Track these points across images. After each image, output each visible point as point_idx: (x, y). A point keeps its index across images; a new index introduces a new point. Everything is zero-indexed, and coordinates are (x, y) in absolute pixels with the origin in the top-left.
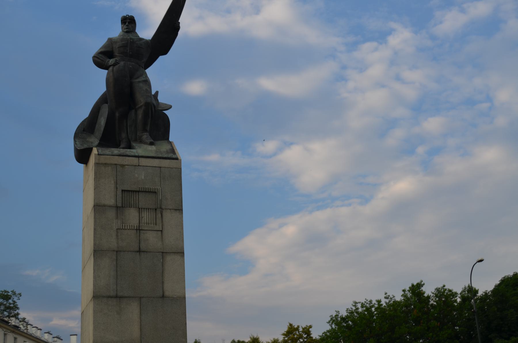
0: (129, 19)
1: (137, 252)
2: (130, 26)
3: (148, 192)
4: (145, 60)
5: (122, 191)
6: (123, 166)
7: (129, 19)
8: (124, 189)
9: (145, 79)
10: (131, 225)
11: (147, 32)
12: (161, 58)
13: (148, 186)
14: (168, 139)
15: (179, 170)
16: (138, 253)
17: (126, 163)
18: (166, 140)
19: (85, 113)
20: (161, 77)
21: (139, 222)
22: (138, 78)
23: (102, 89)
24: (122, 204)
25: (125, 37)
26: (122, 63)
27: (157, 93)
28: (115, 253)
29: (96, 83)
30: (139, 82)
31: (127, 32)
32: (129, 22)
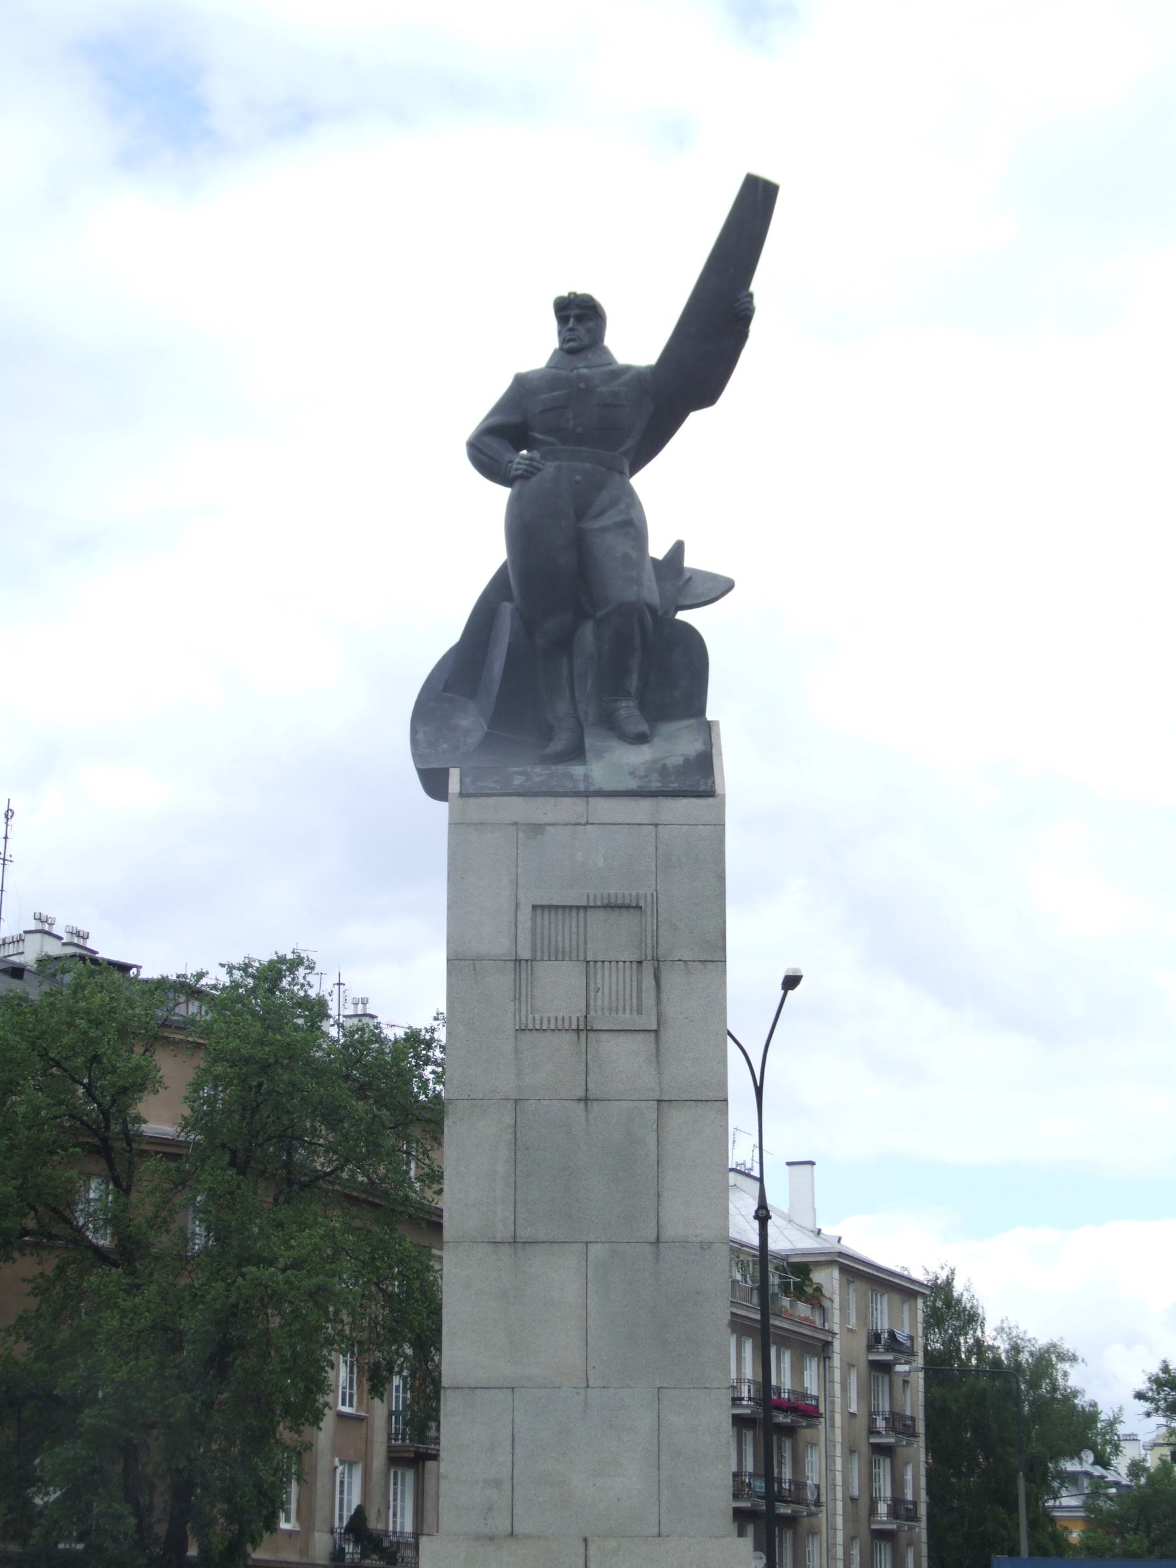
0: (580, 307)
1: (580, 1100)
2: (581, 330)
3: (620, 907)
4: (630, 443)
5: (534, 907)
6: (536, 829)
7: (580, 307)
8: (538, 903)
9: (623, 517)
10: (553, 1015)
11: (638, 338)
12: (696, 420)
13: (616, 890)
14: (702, 711)
15: (719, 826)
16: (582, 1104)
17: (546, 820)
18: (692, 716)
19: (449, 631)
20: (684, 494)
21: (587, 1006)
22: (602, 513)
23: (490, 553)
24: (534, 950)
25: (563, 373)
26: (550, 467)
27: (678, 550)
28: (510, 1105)
29: (469, 535)
30: (604, 529)
31: (571, 352)
32: (580, 317)
